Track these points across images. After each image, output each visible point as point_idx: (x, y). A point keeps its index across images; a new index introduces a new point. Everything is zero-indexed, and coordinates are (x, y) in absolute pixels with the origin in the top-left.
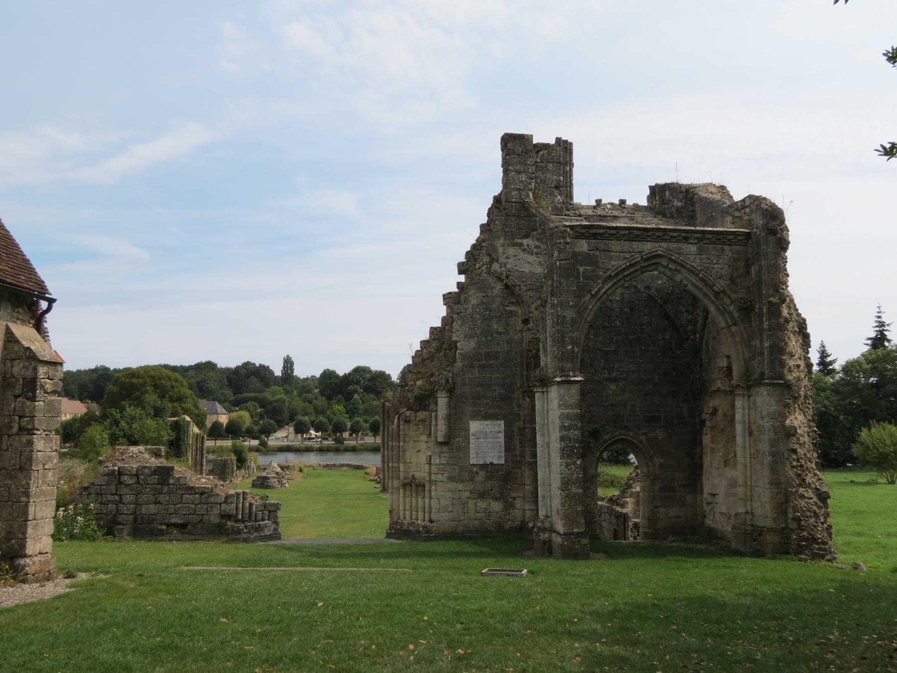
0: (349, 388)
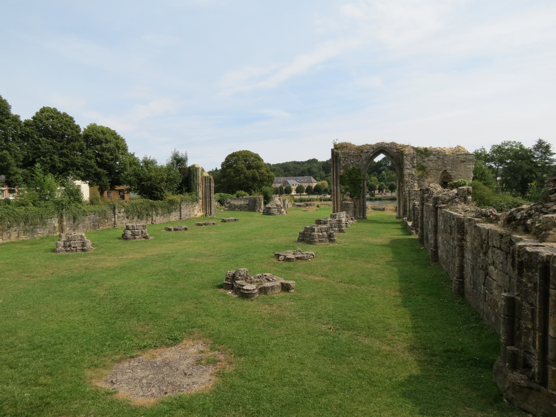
0: (381, 168)
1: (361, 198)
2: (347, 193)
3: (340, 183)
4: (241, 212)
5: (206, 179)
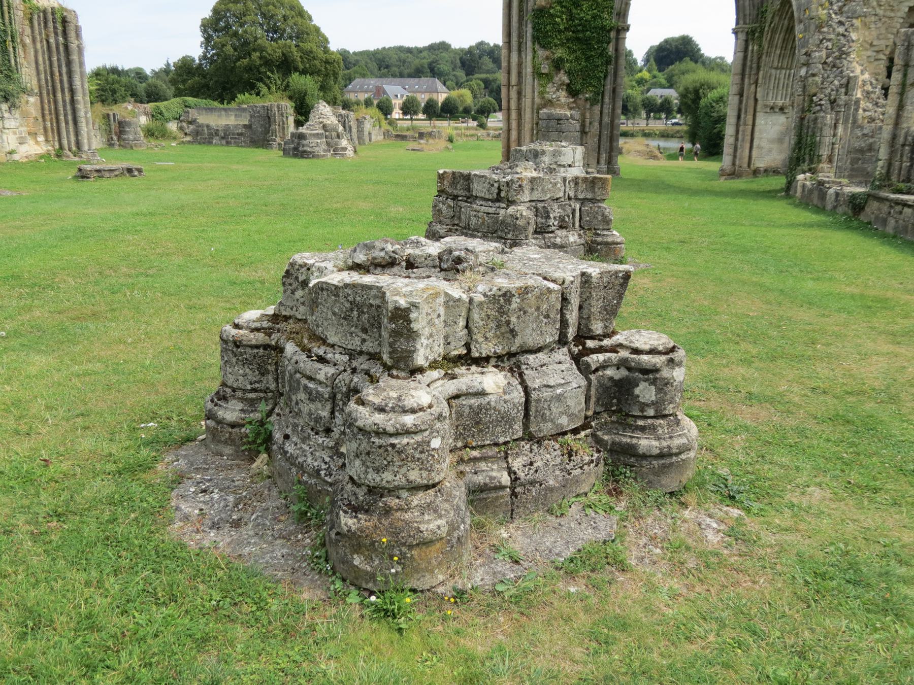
1: (607, 100)
2: (556, 79)
3: (536, 39)
4: (226, 148)
5: (45, 18)
